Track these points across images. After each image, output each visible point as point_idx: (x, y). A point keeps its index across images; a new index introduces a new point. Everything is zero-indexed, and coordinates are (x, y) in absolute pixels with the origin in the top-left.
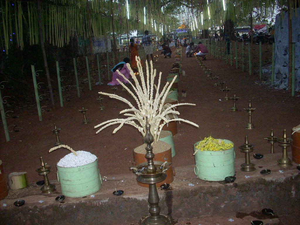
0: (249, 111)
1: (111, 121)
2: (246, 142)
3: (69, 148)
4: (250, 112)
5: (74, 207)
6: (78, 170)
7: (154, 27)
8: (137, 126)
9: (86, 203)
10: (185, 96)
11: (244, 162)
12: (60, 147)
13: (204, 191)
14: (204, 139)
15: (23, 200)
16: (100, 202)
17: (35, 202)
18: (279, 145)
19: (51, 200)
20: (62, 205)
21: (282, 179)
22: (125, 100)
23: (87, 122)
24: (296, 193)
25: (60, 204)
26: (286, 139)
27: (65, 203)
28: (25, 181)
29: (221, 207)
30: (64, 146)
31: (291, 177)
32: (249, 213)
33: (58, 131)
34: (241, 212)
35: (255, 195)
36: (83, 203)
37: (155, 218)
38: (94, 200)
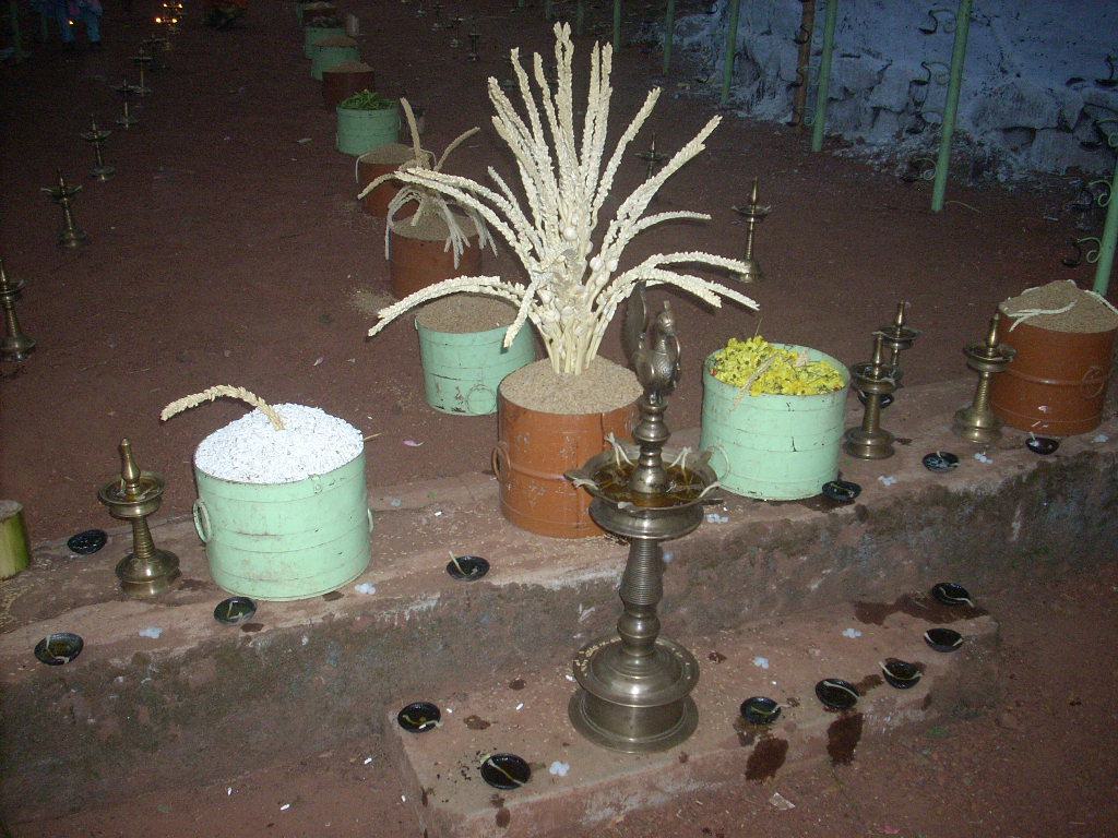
0: (751, 216)
2: (874, 356)
4: (752, 220)
5: (305, 640)
6: (281, 485)
9: (351, 622)
11: (860, 424)
12: (212, 393)
13: (765, 540)
15: (70, 635)
17: (124, 634)
18: (969, 367)
19: (196, 623)
20: (254, 640)
21: (994, 484)
24: (1023, 527)
25: (242, 634)
26: (994, 347)
27: (264, 630)
28: (22, 543)
29: (809, 590)
31: (1019, 477)
32: (892, 603)
34: (866, 600)
35: (914, 542)
36: (340, 624)
37: (635, 658)
38: (382, 605)
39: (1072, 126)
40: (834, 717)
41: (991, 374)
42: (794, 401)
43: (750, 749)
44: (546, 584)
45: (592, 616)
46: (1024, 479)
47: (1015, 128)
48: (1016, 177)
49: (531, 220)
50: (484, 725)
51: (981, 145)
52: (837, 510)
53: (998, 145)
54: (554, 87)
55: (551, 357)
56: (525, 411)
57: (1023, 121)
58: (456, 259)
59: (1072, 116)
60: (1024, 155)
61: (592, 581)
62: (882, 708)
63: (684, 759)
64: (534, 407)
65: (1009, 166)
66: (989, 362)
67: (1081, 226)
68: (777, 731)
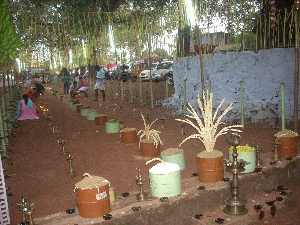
5: (178, 203)
9: (185, 199)
13: (248, 179)
14: (231, 147)
16: (194, 197)
21: (284, 166)
23: (65, 153)
31: (287, 164)
33: (72, 159)
39: (265, 109)
40: (271, 206)
41: (277, 147)
42: (249, 153)
43: (259, 213)
44: (215, 189)
45: (223, 196)
46: (288, 165)
47: (253, 111)
48: (256, 121)
49: (204, 125)
50: (210, 216)
51: (247, 115)
52: (259, 173)
53: (251, 115)
54: (209, 100)
55: (207, 149)
56: (205, 159)
57: (255, 109)
58: (157, 146)
59: (265, 107)
60: (256, 116)
61: (222, 188)
62: (278, 205)
63: (249, 215)
64: (206, 158)
65: (254, 119)
66: (276, 145)
67: (273, 128)
68: (262, 209)
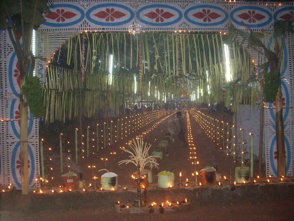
1: (125, 160)
3: (107, 170)
7: (157, 96)
8: (135, 164)
10: (168, 156)
12: (103, 170)
22: (131, 153)
30: (105, 169)
